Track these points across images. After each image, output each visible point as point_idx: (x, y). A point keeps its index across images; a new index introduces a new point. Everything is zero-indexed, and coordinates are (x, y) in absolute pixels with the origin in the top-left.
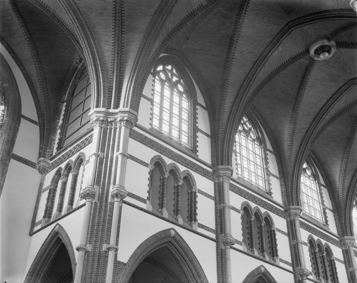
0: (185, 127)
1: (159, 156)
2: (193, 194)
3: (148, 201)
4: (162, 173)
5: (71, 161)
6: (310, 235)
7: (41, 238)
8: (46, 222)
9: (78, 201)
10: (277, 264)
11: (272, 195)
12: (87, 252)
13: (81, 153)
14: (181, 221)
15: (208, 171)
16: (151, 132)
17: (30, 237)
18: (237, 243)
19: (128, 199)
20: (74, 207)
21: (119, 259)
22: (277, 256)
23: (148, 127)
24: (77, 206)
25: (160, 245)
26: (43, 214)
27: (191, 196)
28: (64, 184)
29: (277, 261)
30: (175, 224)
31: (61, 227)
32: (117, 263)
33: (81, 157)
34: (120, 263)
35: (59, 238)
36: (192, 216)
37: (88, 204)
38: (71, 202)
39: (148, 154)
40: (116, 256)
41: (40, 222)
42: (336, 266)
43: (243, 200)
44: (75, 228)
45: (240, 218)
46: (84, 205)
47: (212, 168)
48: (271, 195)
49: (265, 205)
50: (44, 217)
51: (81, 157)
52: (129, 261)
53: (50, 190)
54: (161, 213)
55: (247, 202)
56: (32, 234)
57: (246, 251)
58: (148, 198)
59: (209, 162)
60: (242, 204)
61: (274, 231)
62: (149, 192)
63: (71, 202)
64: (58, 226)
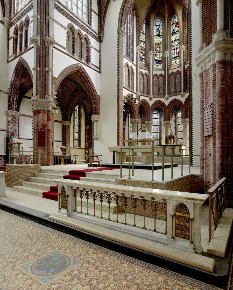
0: (85, 10)
1: (79, 29)
2: (89, 48)
3: (66, 49)
4: (73, 34)
5: (22, 21)
6: (69, 24)
7: (14, 63)
8: (15, 56)
9: (30, 45)
10: (89, 65)
11: (92, 26)
12: (37, 71)
13: (27, 16)
14: (83, 61)
15: (96, 36)
16: (66, 7)
17: (7, 63)
18: (56, 44)
19: (55, 46)
20: (28, 48)
21: (54, 76)
22: (90, 61)
23: (65, 4)
24: (30, 48)
25: (73, 71)
26: (12, 52)
27: (88, 49)
28: (21, 36)
29: (89, 64)
30: (80, 62)
31: (22, 58)
32: (54, 78)
33: (27, 19)
34: (55, 78)
35: (22, 65)
36: (88, 59)
37: (35, 47)
38: (26, 46)
39: (66, 22)
40: (52, 74)
41: (11, 56)
42: (91, 51)
43: (70, 22)
44: (30, 58)
45: (66, 33)
46: (33, 47)
47: (97, 35)
48: (91, 25)
49: (86, 30)
50: (13, 53)
51: (27, 19)
52: (58, 77)
53: (14, 38)
54: (74, 56)
55: (72, 24)
56: (8, 62)
57: (68, 53)
58: (67, 47)
59: (97, 31)
60: (68, 25)
61: (90, 48)
62: (67, 44)
63: (26, 46)
64: (21, 58)
